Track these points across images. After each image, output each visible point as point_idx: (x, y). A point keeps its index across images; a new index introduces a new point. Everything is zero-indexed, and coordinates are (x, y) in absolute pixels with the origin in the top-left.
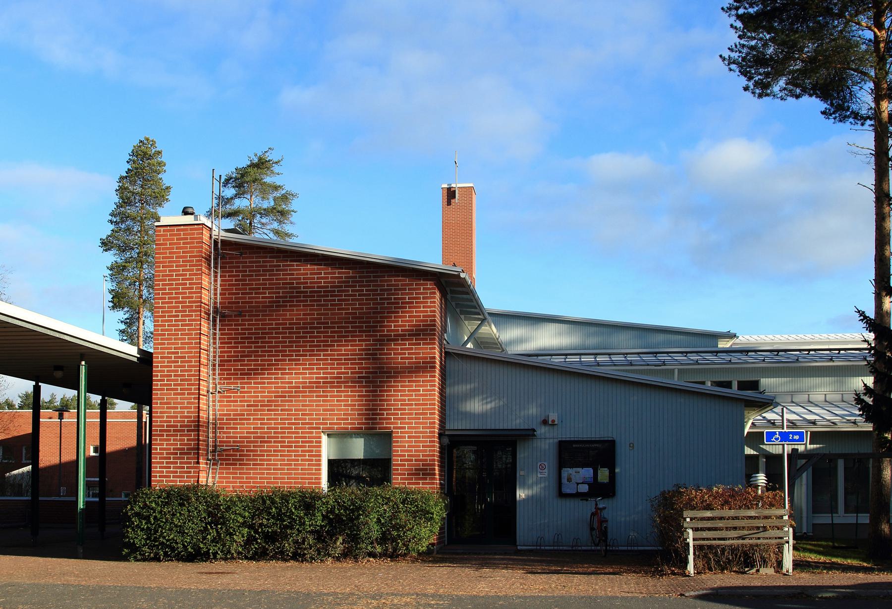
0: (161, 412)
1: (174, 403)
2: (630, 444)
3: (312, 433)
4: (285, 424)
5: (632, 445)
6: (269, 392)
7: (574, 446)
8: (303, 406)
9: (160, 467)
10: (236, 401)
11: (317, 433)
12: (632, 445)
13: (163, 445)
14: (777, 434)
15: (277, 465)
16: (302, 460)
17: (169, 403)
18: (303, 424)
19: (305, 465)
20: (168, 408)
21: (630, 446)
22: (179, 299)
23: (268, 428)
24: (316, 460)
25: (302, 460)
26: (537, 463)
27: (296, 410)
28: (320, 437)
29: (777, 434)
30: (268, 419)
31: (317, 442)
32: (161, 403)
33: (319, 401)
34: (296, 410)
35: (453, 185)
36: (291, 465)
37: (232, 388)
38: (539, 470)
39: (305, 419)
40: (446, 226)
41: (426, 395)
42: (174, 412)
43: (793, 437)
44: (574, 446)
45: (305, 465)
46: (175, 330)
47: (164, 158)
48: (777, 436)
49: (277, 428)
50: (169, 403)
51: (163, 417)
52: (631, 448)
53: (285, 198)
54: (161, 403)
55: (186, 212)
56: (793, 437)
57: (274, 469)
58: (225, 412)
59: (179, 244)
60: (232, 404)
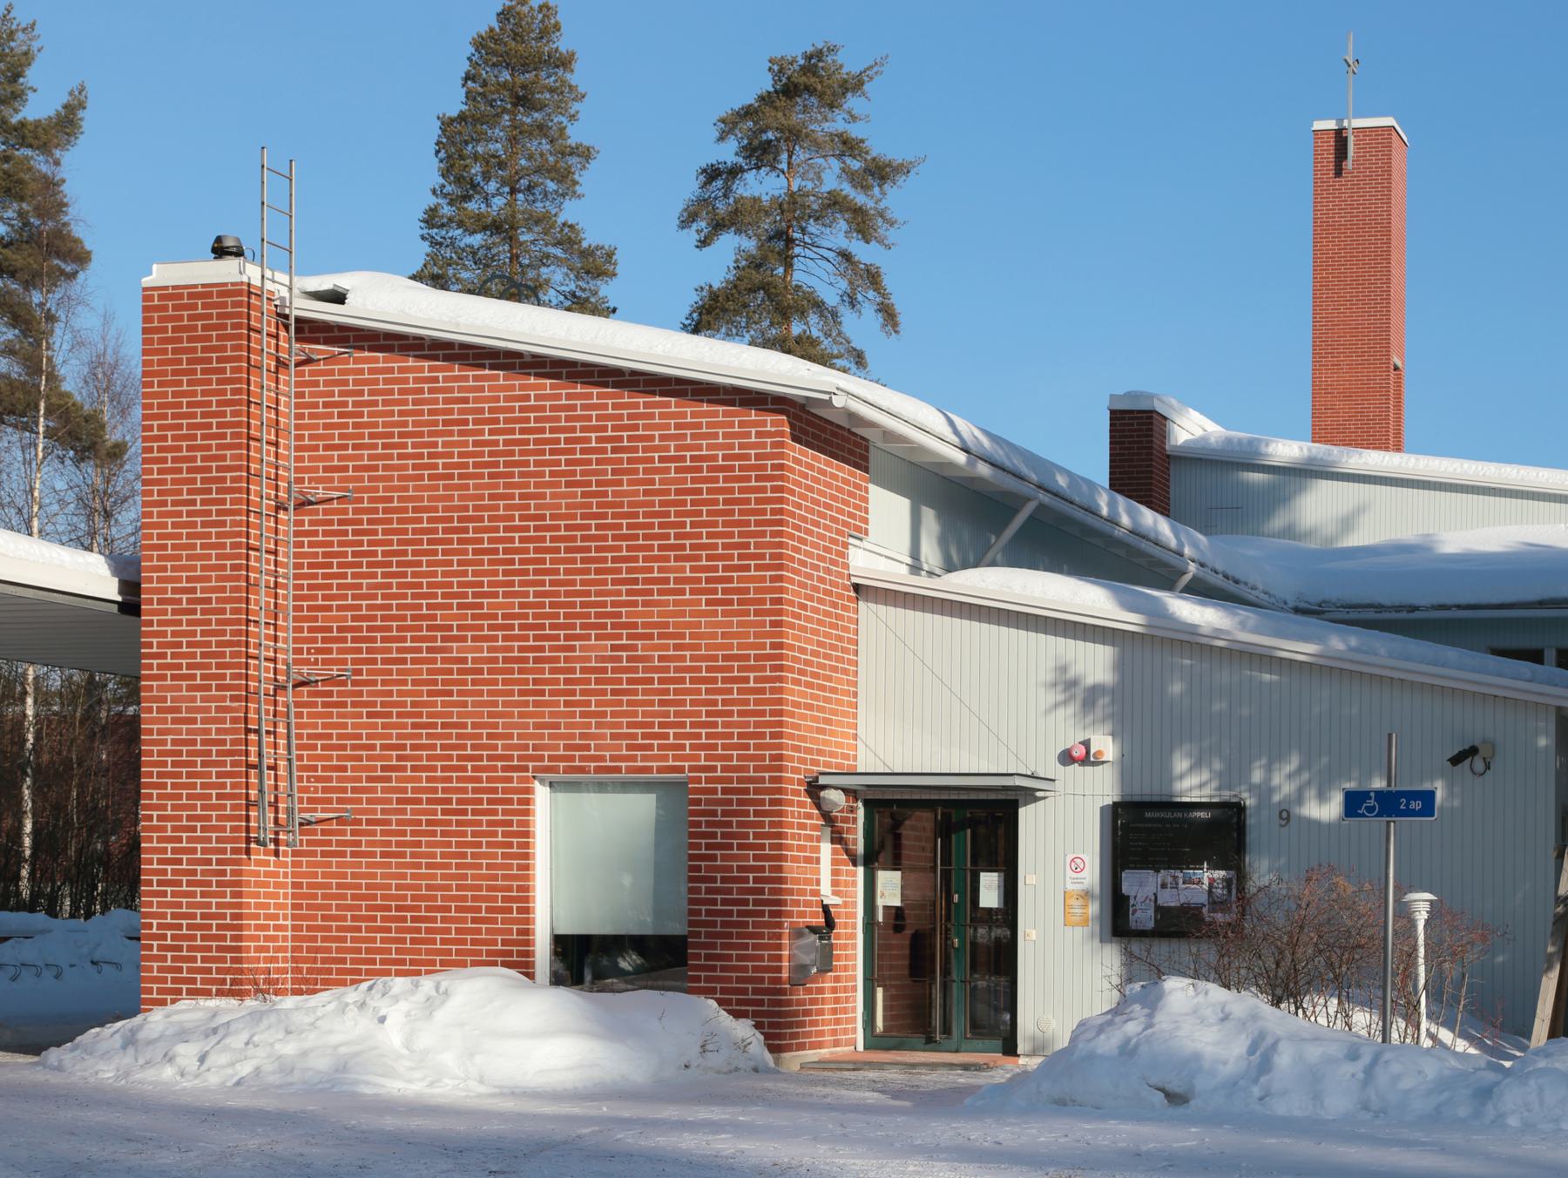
0: (160, 732)
1: (189, 710)
2: (1281, 813)
3: (510, 780)
4: (450, 758)
5: (1284, 815)
6: (415, 683)
7: (1148, 815)
8: (490, 715)
9: (160, 861)
10: (344, 705)
11: (521, 780)
12: (1284, 815)
13: (164, 807)
14: (1371, 798)
15: (433, 856)
16: (489, 845)
17: (178, 710)
18: (490, 758)
19: (494, 856)
20: (175, 721)
21: (1281, 817)
22: (196, 462)
23: (414, 768)
24: (520, 845)
25: (489, 845)
26: (1065, 855)
27: (474, 726)
28: (529, 791)
29: (1371, 798)
30: (414, 747)
31: (520, 801)
32: (160, 710)
33: (526, 704)
34: (474, 726)
35: (1346, 124)
36: (464, 856)
37: (335, 673)
38: (1070, 873)
39: (495, 747)
40: (1322, 229)
41: (762, 690)
42: (189, 732)
43: (1407, 805)
44: (1148, 815)
45: (494, 856)
46: (189, 536)
47: (577, 77)
48: (1372, 802)
49: (434, 769)
50: (178, 710)
51: (164, 742)
52: (1283, 822)
53: (881, 172)
54: (160, 710)
55: (220, 251)
56: (1407, 805)
57: (429, 866)
58: (320, 731)
59: (195, 328)
60: (335, 710)
